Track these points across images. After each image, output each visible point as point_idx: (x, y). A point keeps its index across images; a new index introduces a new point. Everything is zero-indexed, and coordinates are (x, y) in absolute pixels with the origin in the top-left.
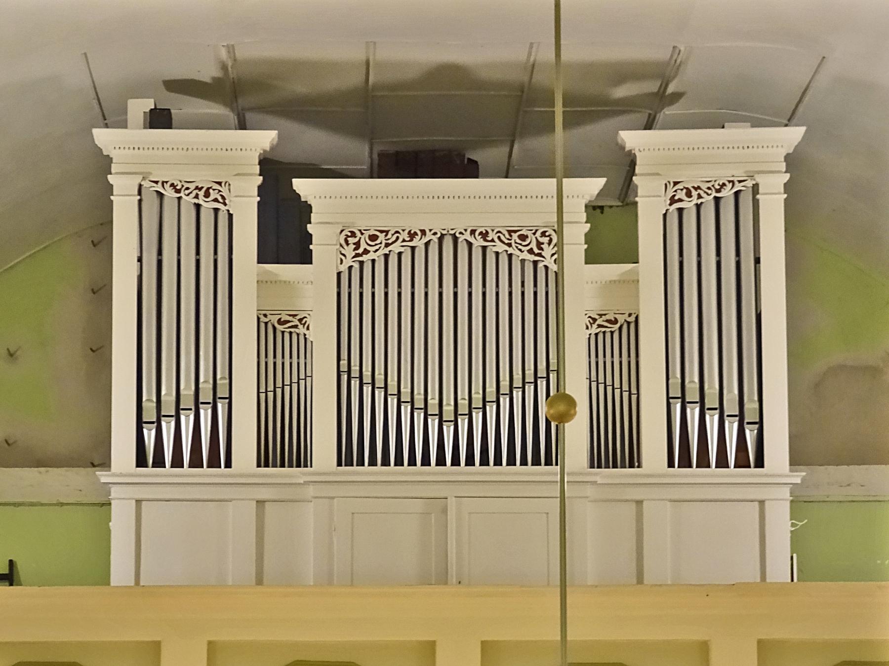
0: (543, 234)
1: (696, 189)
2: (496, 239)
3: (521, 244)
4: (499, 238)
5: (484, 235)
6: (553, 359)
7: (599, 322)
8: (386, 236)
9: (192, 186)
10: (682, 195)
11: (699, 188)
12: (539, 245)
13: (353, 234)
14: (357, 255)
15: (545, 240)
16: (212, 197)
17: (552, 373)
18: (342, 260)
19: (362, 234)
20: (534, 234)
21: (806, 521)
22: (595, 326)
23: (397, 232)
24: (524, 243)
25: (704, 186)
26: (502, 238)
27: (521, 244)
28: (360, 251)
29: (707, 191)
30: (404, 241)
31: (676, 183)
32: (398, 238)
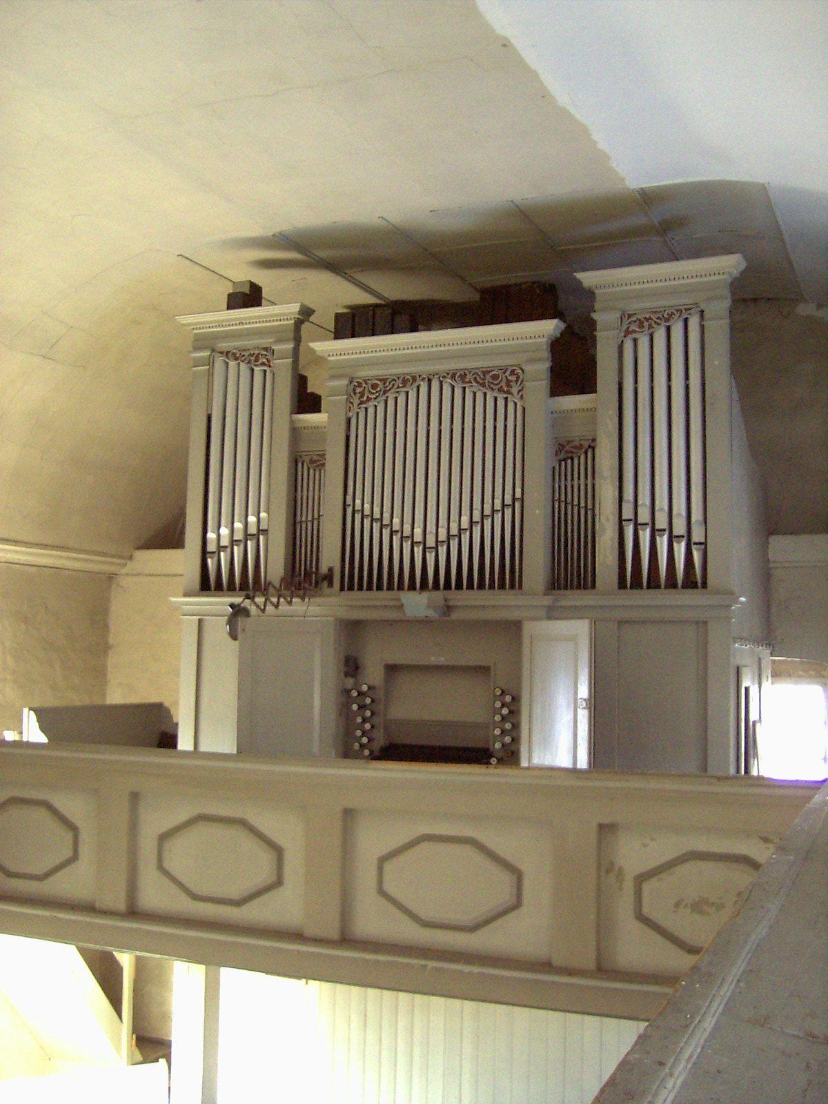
0: (512, 373)
1: (647, 319)
2: (472, 380)
3: (492, 383)
4: (475, 379)
5: (463, 377)
6: (387, 512)
7: (567, 448)
8: (385, 384)
9: (246, 354)
10: (633, 327)
11: (650, 318)
12: (508, 383)
13: (360, 385)
14: (361, 403)
15: (513, 378)
16: (260, 361)
17: (237, 545)
18: (350, 408)
19: (366, 383)
20: (504, 373)
21: (173, 599)
22: (563, 452)
23: (394, 380)
24: (495, 382)
25: (654, 317)
26: (478, 379)
27: (492, 383)
28: (365, 398)
29: (658, 321)
30: (398, 387)
31: (630, 316)
32: (393, 385)
